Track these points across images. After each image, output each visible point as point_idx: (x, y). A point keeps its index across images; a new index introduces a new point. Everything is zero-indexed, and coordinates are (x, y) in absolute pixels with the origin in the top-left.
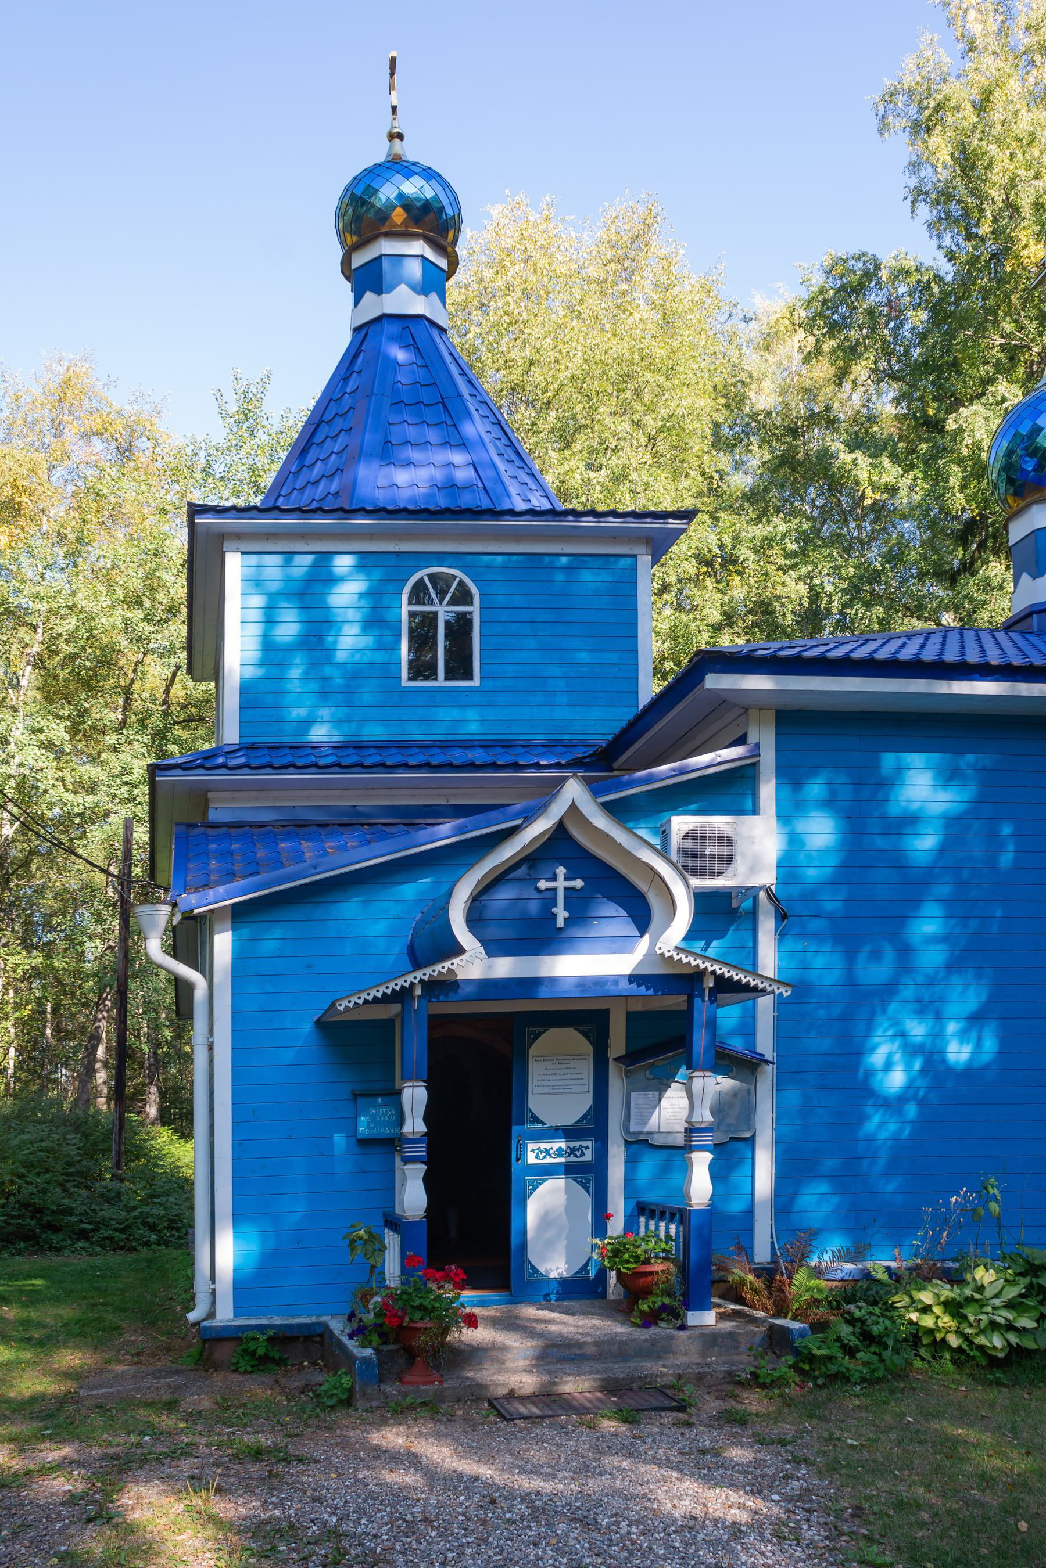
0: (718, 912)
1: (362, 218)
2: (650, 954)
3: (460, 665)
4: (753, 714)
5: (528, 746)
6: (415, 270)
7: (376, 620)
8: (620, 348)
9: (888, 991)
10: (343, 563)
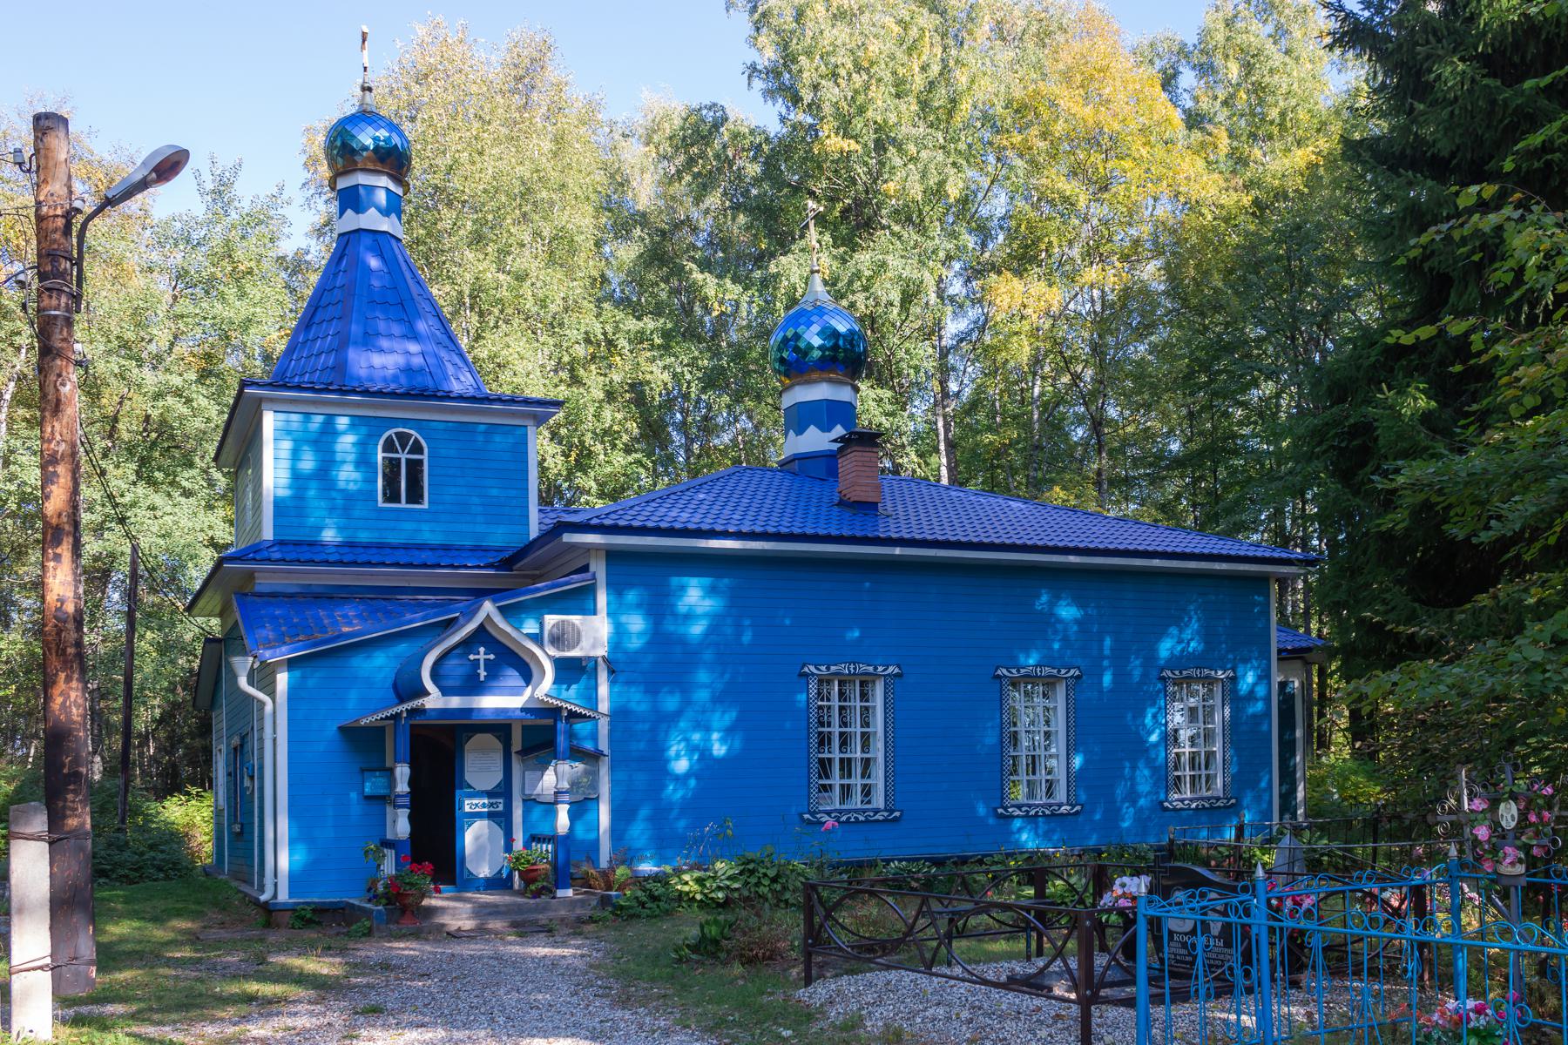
0: (570, 670)
1: (342, 151)
2: (532, 696)
3: (415, 495)
4: (593, 553)
5: (460, 549)
6: (381, 197)
7: (364, 462)
8: (524, 171)
9: (678, 714)
10: (343, 422)
